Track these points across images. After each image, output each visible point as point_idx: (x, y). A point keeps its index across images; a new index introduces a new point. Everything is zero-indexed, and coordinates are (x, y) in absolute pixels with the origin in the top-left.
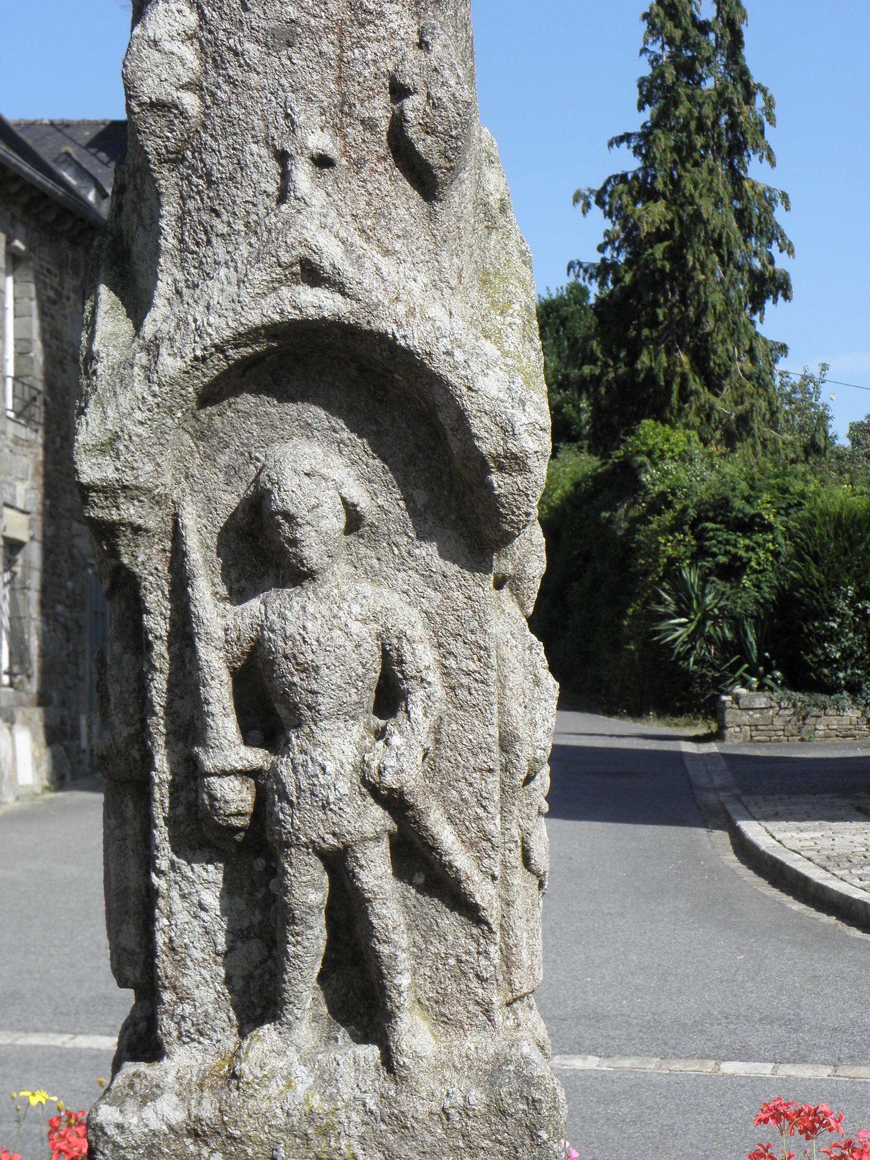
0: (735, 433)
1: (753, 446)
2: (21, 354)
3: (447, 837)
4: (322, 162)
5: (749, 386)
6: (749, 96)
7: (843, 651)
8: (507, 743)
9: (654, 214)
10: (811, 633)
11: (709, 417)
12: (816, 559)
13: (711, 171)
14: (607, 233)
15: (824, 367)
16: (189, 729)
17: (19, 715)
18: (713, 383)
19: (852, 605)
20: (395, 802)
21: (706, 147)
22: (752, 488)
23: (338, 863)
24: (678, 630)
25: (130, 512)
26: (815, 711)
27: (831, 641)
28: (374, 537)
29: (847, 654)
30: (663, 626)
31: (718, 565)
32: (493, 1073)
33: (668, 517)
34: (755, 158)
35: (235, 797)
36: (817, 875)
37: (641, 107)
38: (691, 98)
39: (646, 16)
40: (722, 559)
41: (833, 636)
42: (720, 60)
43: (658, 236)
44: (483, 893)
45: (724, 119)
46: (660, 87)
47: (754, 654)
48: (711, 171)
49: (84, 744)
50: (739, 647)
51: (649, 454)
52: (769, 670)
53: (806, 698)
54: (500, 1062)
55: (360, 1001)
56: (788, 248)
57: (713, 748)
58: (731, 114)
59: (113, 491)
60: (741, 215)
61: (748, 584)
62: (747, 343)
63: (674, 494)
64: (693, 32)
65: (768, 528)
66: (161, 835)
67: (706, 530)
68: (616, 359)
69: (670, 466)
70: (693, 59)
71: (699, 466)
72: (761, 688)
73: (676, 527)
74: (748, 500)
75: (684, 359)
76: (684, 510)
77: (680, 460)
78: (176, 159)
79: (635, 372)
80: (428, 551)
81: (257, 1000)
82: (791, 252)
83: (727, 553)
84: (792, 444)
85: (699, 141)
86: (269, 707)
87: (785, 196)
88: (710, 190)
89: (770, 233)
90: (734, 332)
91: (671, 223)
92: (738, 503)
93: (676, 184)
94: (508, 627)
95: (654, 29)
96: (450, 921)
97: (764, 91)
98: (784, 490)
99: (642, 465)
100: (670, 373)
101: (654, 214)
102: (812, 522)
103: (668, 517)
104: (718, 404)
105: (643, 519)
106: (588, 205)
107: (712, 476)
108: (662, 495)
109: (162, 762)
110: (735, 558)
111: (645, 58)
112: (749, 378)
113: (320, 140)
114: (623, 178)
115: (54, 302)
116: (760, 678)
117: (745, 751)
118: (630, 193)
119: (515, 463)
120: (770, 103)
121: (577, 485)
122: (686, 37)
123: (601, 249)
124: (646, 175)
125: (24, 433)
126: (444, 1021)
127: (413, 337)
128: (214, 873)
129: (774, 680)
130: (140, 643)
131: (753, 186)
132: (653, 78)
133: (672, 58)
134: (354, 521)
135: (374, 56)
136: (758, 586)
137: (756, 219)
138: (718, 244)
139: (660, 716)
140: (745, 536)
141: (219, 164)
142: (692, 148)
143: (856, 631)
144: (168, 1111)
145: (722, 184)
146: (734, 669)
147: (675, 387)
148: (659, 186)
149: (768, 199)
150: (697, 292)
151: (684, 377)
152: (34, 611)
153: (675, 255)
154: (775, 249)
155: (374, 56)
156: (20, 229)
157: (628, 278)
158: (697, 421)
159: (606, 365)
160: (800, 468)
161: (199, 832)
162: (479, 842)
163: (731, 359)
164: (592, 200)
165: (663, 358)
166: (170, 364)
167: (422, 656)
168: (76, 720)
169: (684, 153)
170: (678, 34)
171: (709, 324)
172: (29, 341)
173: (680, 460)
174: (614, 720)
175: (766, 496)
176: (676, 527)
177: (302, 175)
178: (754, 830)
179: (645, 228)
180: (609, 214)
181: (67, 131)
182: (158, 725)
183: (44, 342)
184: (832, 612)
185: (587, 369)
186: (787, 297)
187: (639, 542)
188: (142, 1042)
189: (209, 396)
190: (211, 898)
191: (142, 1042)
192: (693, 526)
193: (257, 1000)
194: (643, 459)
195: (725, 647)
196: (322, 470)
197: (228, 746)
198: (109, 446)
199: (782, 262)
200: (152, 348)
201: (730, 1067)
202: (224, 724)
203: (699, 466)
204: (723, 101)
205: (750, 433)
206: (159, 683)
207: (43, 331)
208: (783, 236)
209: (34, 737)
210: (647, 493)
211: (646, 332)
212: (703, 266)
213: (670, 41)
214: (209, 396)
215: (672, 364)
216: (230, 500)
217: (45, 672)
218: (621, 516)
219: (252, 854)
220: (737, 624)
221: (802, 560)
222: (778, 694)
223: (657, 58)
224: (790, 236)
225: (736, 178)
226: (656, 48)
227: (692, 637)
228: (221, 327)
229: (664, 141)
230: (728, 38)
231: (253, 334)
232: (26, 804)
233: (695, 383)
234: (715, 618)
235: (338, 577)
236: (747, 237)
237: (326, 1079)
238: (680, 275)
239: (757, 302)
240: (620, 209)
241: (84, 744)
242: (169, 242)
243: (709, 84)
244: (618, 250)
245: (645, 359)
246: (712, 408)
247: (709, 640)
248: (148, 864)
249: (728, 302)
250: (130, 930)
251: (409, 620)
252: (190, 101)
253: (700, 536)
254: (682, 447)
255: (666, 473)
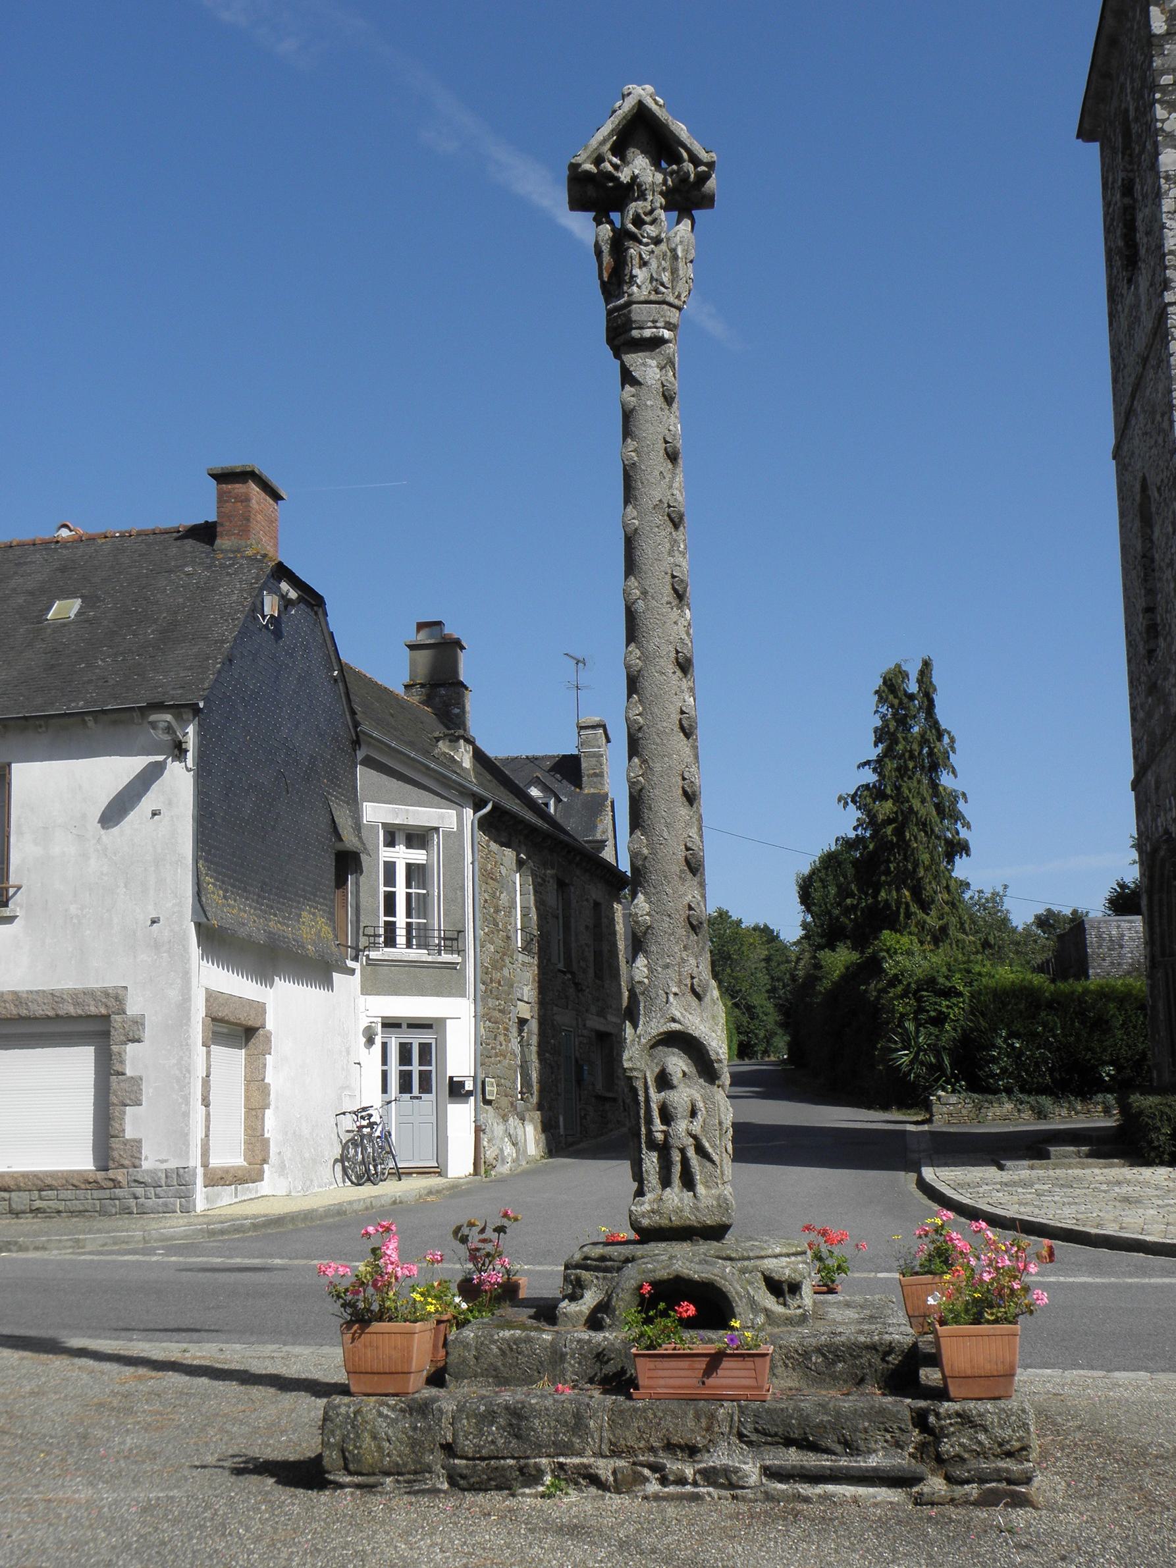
0: (939, 936)
1: (951, 944)
2: (525, 915)
3: (707, 1145)
4: (676, 994)
5: (947, 909)
6: (940, 736)
7: (1001, 1069)
8: (720, 1123)
9: (886, 808)
10: (981, 1059)
11: (923, 928)
12: (983, 1014)
13: (919, 782)
14: (858, 820)
15: (1006, 887)
16: (649, 1121)
17: (527, 1116)
18: (925, 906)
19: (1005, 1041)
20: (695, 1137)
21: (915, 767)
22: (949, 970)
23: (683, 1151)
24: (904, 1057)
25: (635, 1074)
26: (986, 1105)
27: (994, 1063)
28: (689, 1078)
29: (1004, 1070)
30: (894, 1056)
31: (930, 1017)
32: (718, 1198)
33: (900, 988)
34: (945, 772)
35: (660, 1137)
36: (949, 1192)
37: (876, 745)
38: (905, 739)
39: (876, 692)
40: (933, 1014)
41: (994, 1060)
42: (922, 715)
43: (889, 821)
44: (716, 1158)
45: (925, 750)
46: (888, 732)
47: (949, 1071)
48: (919, 782)
49: (562, 1131)
50: (938, 1067)
51: (888, 951)
52: (958, 1081)
53: (980, 1097)
54: (720, 1195)
55: (688, 1182)
56: (967, 825)
57: (926, 1127)
58: (929, 747)
59: (631, 1069)
60: (939, 808)
61: (949, 1028)
62: (944, 882)
63: (903, 975)
64: (905, 700)
65: (960, 994)
66: (643, 1146)
67: (923, 996)
68: (866, 894)
69: (900, 958)
70: (906, 716)
71: (918, 958)
72: (953, 1091)
73: (905, 994)
74: (947, 978)
75: (907, 893)
76: (909, 984)
77: (907, 954)
78: (643, 993)
79: (878, 902)
80: (701, 1081)
81: (666, 1182)
82: (969, 827)
83: (935, 1010)
84: (974, 942)
85: (911, 765)
86: (667, 1117)
87: (964, 794)
88: (918, 793)
89: (957, 817)
90: (936, 877)
91: (896, 813)
92: (941, 980)
93: (898, 788)
94: (720, 1096)
95: (882, 699)
96: (708, 1164)
97: (949, 733)
98: (969, 971)
99: (884, 958)
100: (899, 902)
101: (886, 808)
102: (980, 993)
103: (900, 988)
104: (928, 919)
105: (884, 991)
106: (846, 804)
107: (925, 964)
108: (896, 975)
109: (643, 1129)
110: (941, 1012)
111: (877, 716)
112: (947, 903)
113: (675, 989)
114: (867, 787)
115: (541, 885)
116: (953, 1085)
117: (944, 1130)
118: (871, 796)
119: (720, 1061)
120: (952, 740)
121: (847, 968)
122: (901, 703)
123: (855, 829)
124: (881, 785)
125: (527, 959)
126: (707, 1187)
127: (696, 1034)
128: (655, 1154)
129: (961, 1086)
130: (638, 1103)
131: (945, 789)
132: (882, 729)
133: (894, 715)
134: (684, 1074)
135: (686, 970)
136: (954, 1029)
137: (947, 808)
138: (924, 824)
139: (899, 1109)
140: (946, 1000)
141: (653, 995)
142: (907, 768)
143: (1008, 1057)
144: (647, 1207)
145: (926, 792)
146: (937, 1080)
147: (902, 910)
148: (888, 791)
149: (954, 797)
150: (913, 854)
151: (907, 904)
152: (534, 1058)
153: (899, 832)
154: (959, 826)
155: (686, 970)
156: (524, 848)
157: (871, 846)
158: (916, 930)
159: (860, 898)
160: (979, 957)
161: (652, 1145)
162: (714, 1146)
163: (935, 892)
164: (849, 800)
165: (894, 893)
166: (643, 1041)
167: (700, 1105)
168: (558, 1118)
169: (902, 771)
170: (896, 702)
171: (921, 873)
172: (528, 908)
173: (907, 954)
174: (871, 1112)
175: (958, 976)
176: (905, 994)
177: (671, 998)
178: (928, 1173)
179: (881, 817)
180: (859, 808)
181: (537, 762)
182: (642, 1121)
183: (537, 909)
184: (994, 1046)
185: (849, 901)
186: (968, 855)
187: (883, 1005)
188: (640, 1193)
189: (652, 1047)
190: (655, 1160)
191: (640, 1193)
192: (914, 995)
193: (666, 1182)
194: (885, 954)
195: (931, 1068)
196: (677, 1063)
197: (658, 1126)
198: (630, 1059)
199: (964, 834)
200: (639, 1037)
201: (880, 1275)
202: (657, 1121)
203: (918, 958)
204: (924, 741)
205: (947, 935)
206: (642, 1112)
207: (536, 900)
208: (964, 818)
209: (535, 1129)
210: (887, 974)
211: (883, 878)
212: (916, 838)
213: (892, 706)
214: (652, 1047)
215: (900, 897)
216: (657, 1070)
217: (542, 1091)
218: (872, 988)
219: (663, 1150)
220: (938, 1056)
221: (974, 1015)
222: (964, 1094)
223: (884, 716)
224: (968, 818)
225: (934, 785)
226: (884, 710)
227: (912, 1062)
228: (654, 1032)
229: (891, 765)
230: (926, 703)
231: (661, 1034)
232: (533, 1165)
233: (914, 908)
234: (925, 1050)
235: (681, 1087)
236: (943, 819)
237: (681, 1200)
238: (903, 845)
239: (950, 858)
240: (865, 805)
241: (562, 1131)
242: (642, 1012)
243: (916, 729)
244: (865, 829)
245: (883, 894)
246: (925, 922)
247: (922, 1063)
248: (640, 1152)
249: (932, 859)
250: (636, 1168)
251: (697, 1096)
252: (646, 981)
253: (919, 1000)
254: (907, 946)
255: (898, 962)
